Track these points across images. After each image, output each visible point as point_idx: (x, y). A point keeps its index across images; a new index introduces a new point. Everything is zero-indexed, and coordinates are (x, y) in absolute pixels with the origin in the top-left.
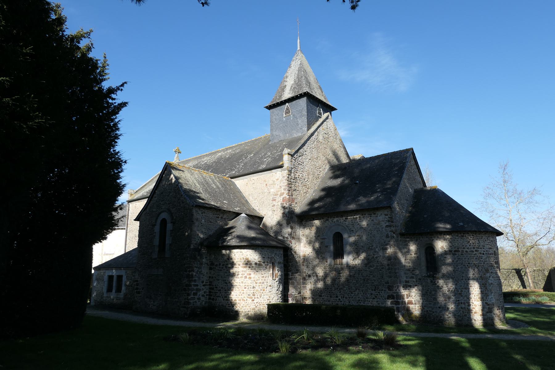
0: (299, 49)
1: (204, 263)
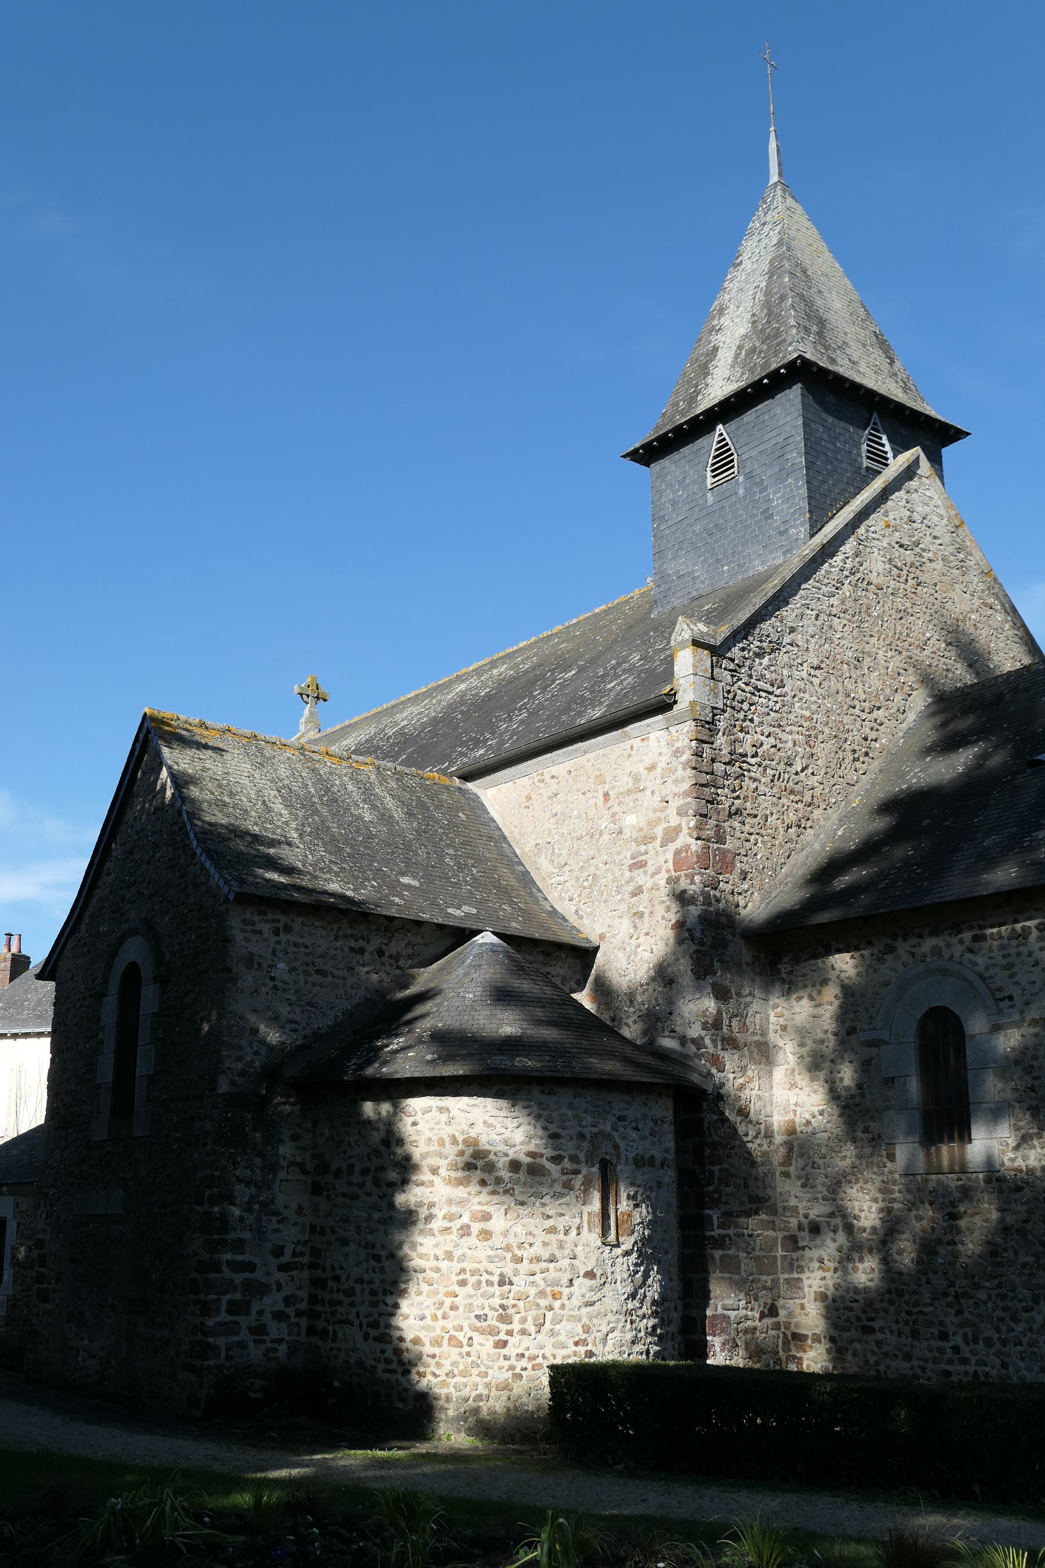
0: (774, 178)
1: (284, 1163)
